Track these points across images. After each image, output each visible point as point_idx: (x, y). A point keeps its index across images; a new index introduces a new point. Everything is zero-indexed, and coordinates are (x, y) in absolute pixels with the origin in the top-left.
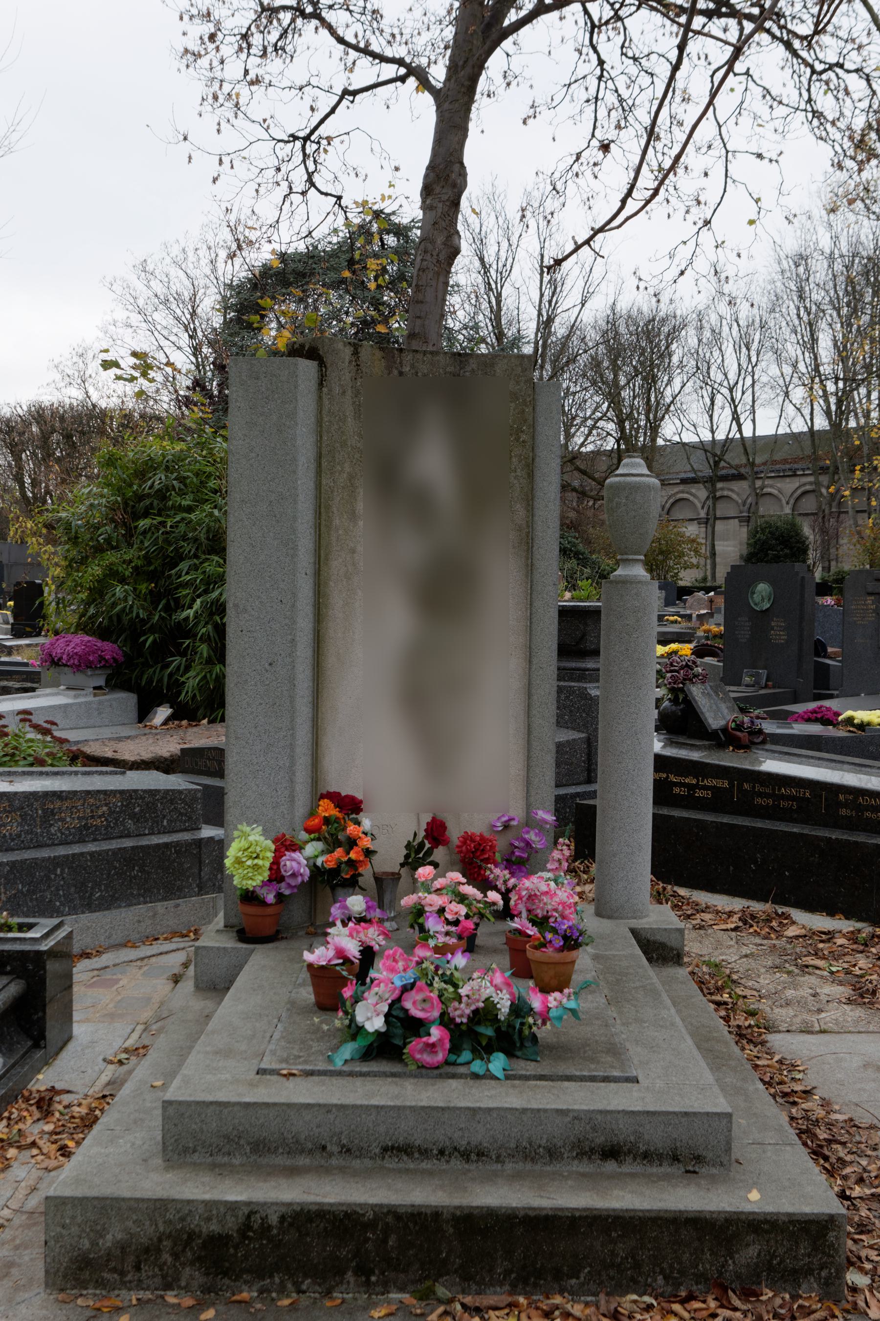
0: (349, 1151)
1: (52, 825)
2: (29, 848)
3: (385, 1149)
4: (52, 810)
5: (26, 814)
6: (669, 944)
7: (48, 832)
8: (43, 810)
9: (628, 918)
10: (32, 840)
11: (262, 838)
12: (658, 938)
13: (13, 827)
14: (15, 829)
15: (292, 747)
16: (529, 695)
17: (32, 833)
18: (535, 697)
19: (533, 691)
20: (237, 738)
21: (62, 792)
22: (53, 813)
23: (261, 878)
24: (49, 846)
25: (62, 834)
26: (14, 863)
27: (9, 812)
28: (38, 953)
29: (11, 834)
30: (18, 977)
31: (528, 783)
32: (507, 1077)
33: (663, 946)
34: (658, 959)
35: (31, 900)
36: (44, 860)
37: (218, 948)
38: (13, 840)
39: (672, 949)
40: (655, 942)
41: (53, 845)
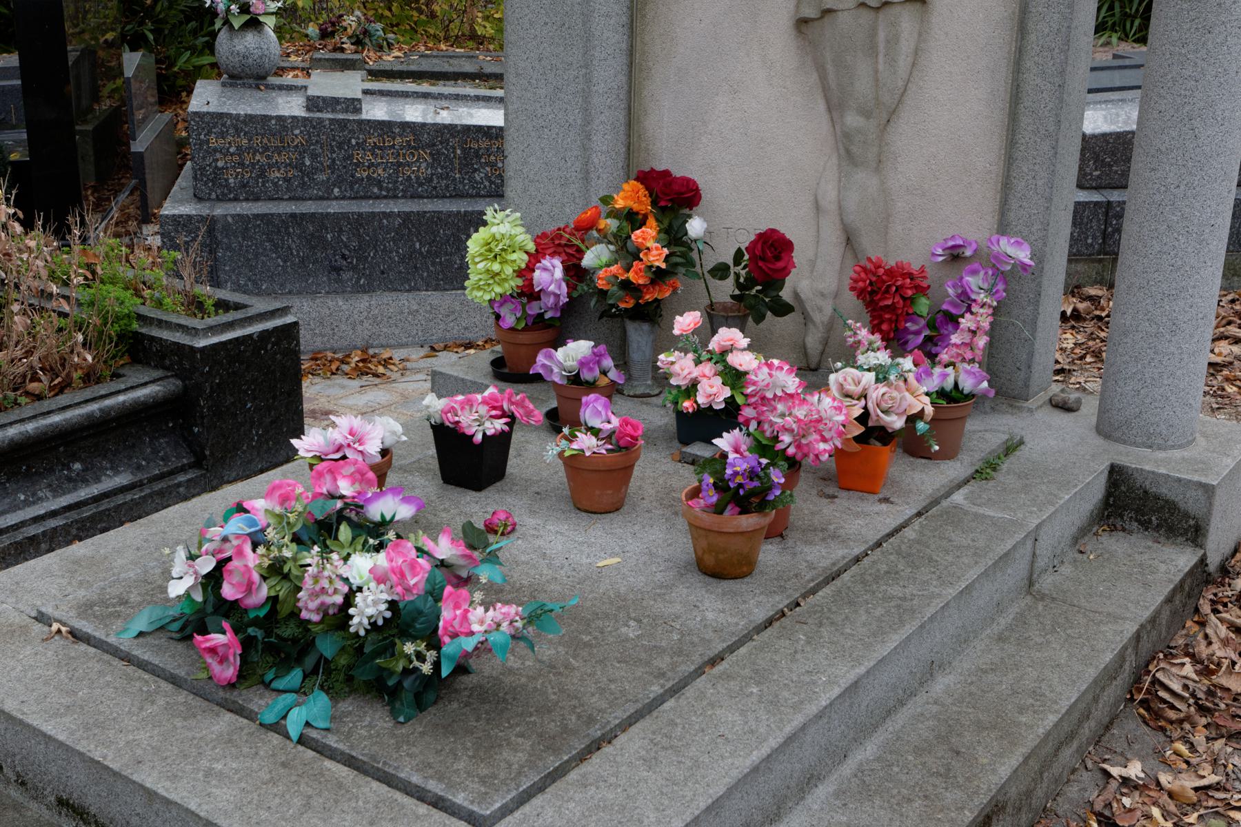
0: (23, 784)
1: (476, 170)
2: (444, 197)
3: (62, 803)
4: (477, 152)
5: (438, 152)
6: (1182, 505)
7: (471, 179)
8: (463, 150)
9: (1135, 444)
10: (447, 186)
11: (520, 230)
12: (1163, 490)
13: (421, 167)
14: (424, 170)
15: (586, 96)
16: (1022, 29)
17: (447, 177)
18: (1033, 37)
19: (1031, 25)
20: (518, 75)
21: (490, 128)
22: (478, 156)
23: (498, 290)
24: (472, 196)
25: (491, 182)
26: (408, 214)
27: (416, 149)
28: (192, 348)
29: (418, 178)
30: (176, 376)
31: (1006, 186)
32: (302, 740)
33: (1171, 506)
34: (1159, 527)
35: (433, 264)
36: (450, 214)
37: (456, 378)
38: (421, 185)
39: (1187, 515)
40: (1157, 497)
41: (478, 195)
